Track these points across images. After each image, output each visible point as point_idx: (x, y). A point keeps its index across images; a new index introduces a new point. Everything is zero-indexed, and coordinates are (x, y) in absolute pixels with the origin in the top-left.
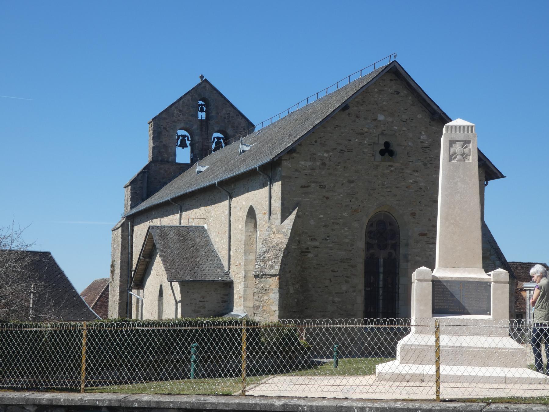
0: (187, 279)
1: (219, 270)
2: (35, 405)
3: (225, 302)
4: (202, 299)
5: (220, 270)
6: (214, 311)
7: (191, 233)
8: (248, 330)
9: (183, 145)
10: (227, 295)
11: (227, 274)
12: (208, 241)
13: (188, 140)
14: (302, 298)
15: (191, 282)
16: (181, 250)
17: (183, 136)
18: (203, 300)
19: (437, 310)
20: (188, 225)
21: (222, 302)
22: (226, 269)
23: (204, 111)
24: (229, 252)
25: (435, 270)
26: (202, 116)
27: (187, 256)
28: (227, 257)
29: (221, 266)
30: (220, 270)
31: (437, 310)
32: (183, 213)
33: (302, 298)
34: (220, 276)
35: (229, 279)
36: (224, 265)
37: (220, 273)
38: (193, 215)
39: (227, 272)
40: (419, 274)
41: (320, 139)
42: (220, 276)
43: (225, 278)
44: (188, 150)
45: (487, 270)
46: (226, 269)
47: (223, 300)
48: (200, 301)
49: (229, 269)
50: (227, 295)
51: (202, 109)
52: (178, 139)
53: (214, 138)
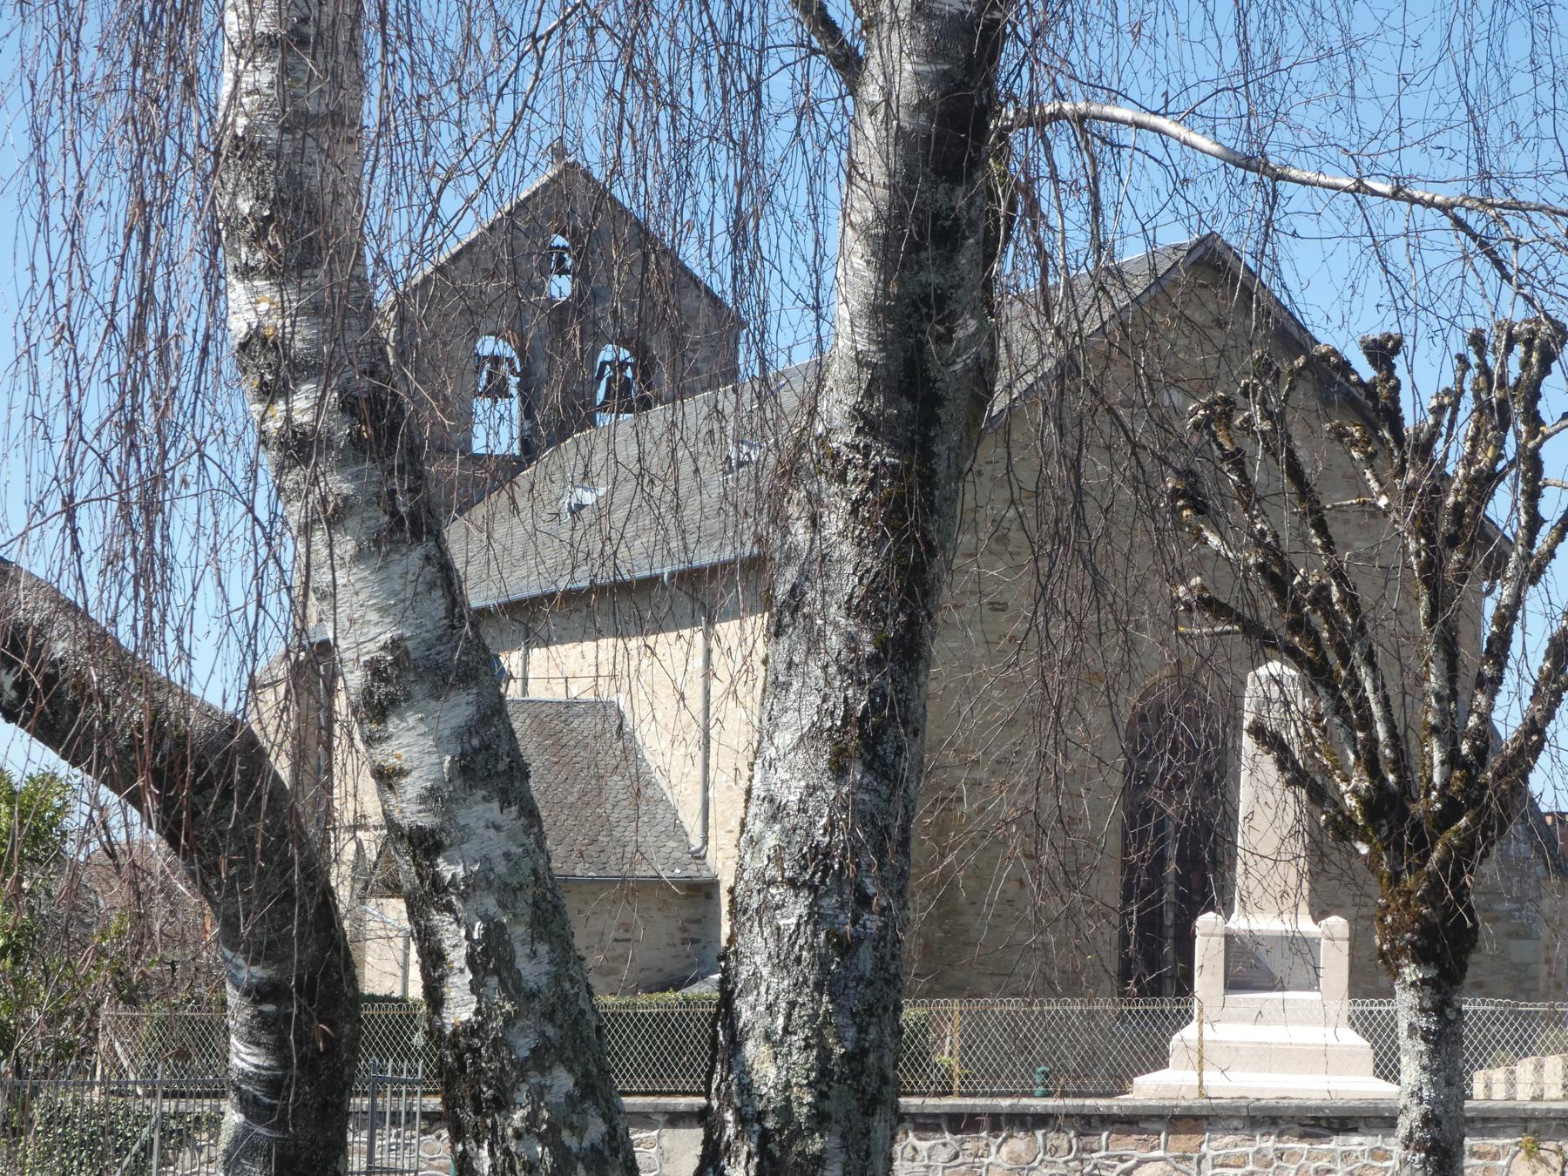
0: (578, 872)
1: (672, 844)
2: (666, 1113)
3: (694, 941)
4: (622, 935)
5: (674, 844)
6: (660, 970)
7: (576, 722)
8: (961, 1013)
9: (498, 391)
10: (697, 921)
11: (698, 857)
12: (630, 753)
13: (513, 371)
14: (940, 934)
15: (592, 881)
16: (550, 778)
17: (496, 360)
18: (628, 936)
19: (1234, 984)
20: (563, 698)
21: (684, 942)
22: (696, 842)
23: (566, 272)
24: (706, 789)
25: (1234, 917)
26: (561, 287)
27: (571, 799)
28: (698, 805)
29: (677, 829)
30: (674, 844)
31: (1234, 984)
32: (536, 650)
33: (940, 934)
34: (676, 863)
35: (705, 873)
36: (688, 829)
37: (677, 854)
38: (572, 660)
39: (698, 851)
40: (1206, 924)
41: (990, 467)
42: (676, 863)
43: (692, 871)
44: (513, 406)
45: (1318, 914)
46: (696, 842)
47: (686, 935)
48: (616, 940)
49: (706, 841)
50: (697, 921)
51: (561, 260)
52: (478, 371)
53: (604, 364)
